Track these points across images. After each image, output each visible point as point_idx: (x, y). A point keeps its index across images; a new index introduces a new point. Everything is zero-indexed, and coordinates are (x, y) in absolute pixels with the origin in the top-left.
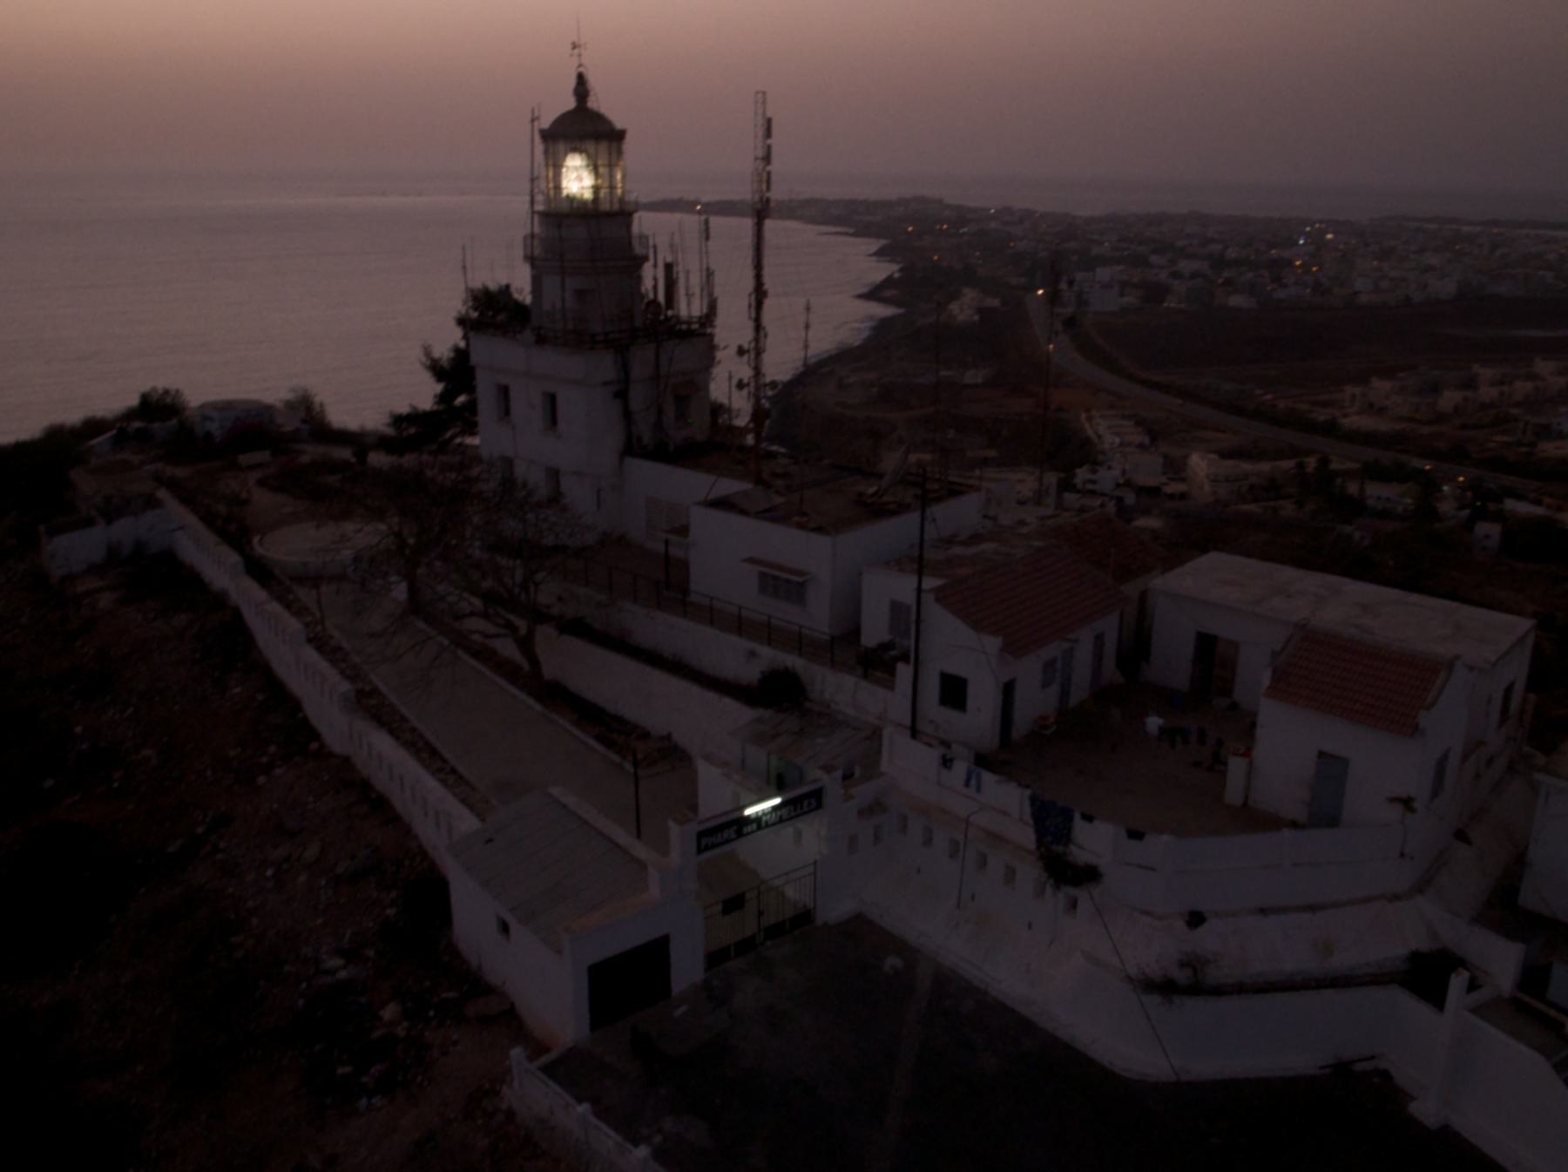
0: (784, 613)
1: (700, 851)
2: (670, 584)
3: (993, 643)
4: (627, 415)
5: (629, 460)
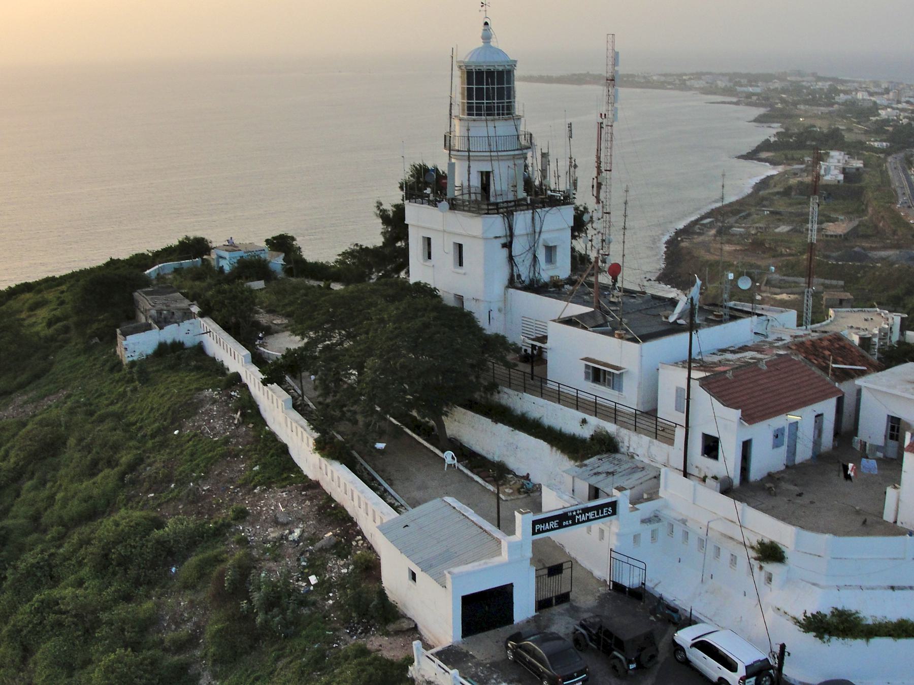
0: (603, 393)
1: (534, 533)
4: (511, 258)
5: (512, 290)
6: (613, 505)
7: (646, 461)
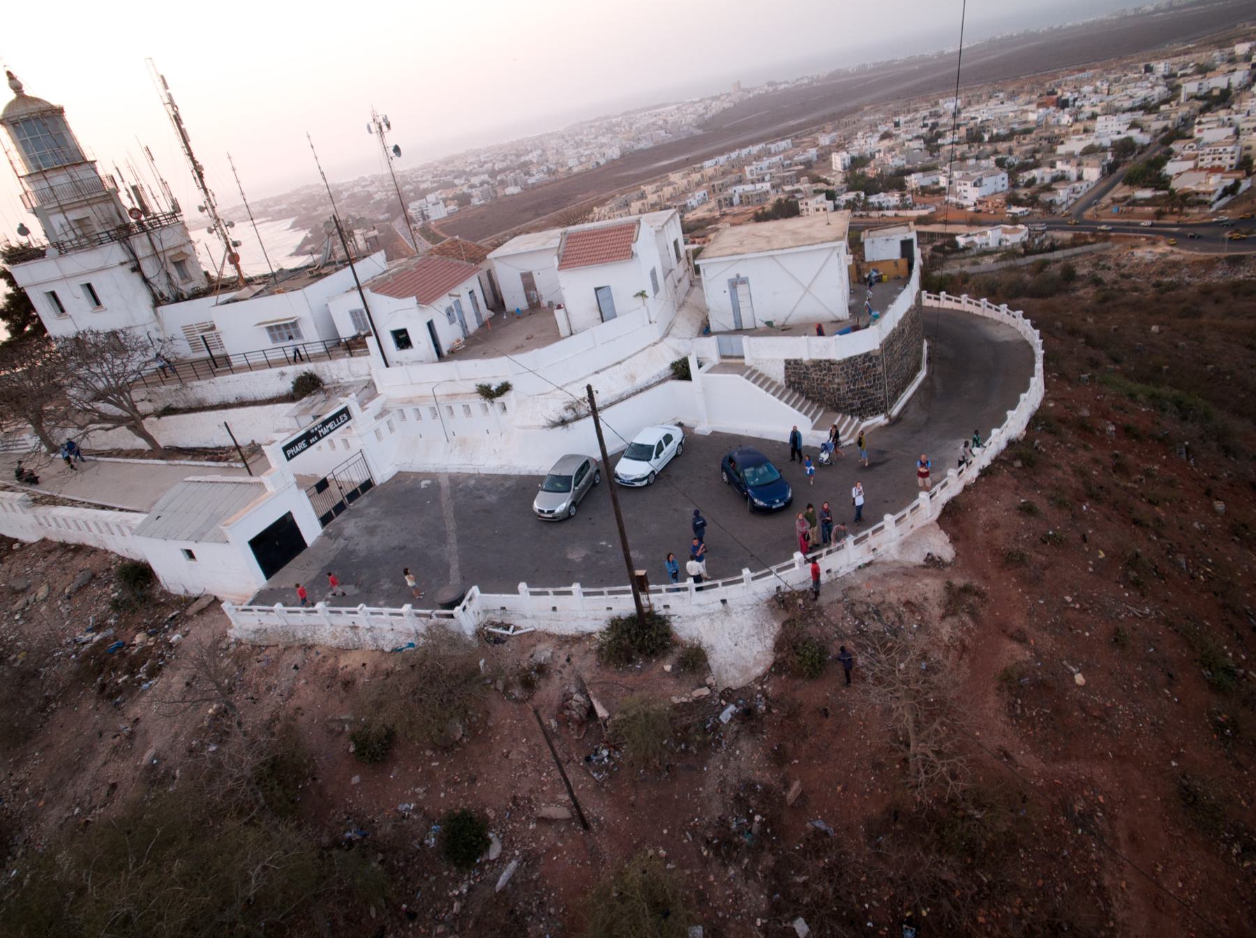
2: (219, 364)
3: (412, 301)
4: (146, 280)
5: (159, 309)
6: (345, 411)
7: (352, 379)
